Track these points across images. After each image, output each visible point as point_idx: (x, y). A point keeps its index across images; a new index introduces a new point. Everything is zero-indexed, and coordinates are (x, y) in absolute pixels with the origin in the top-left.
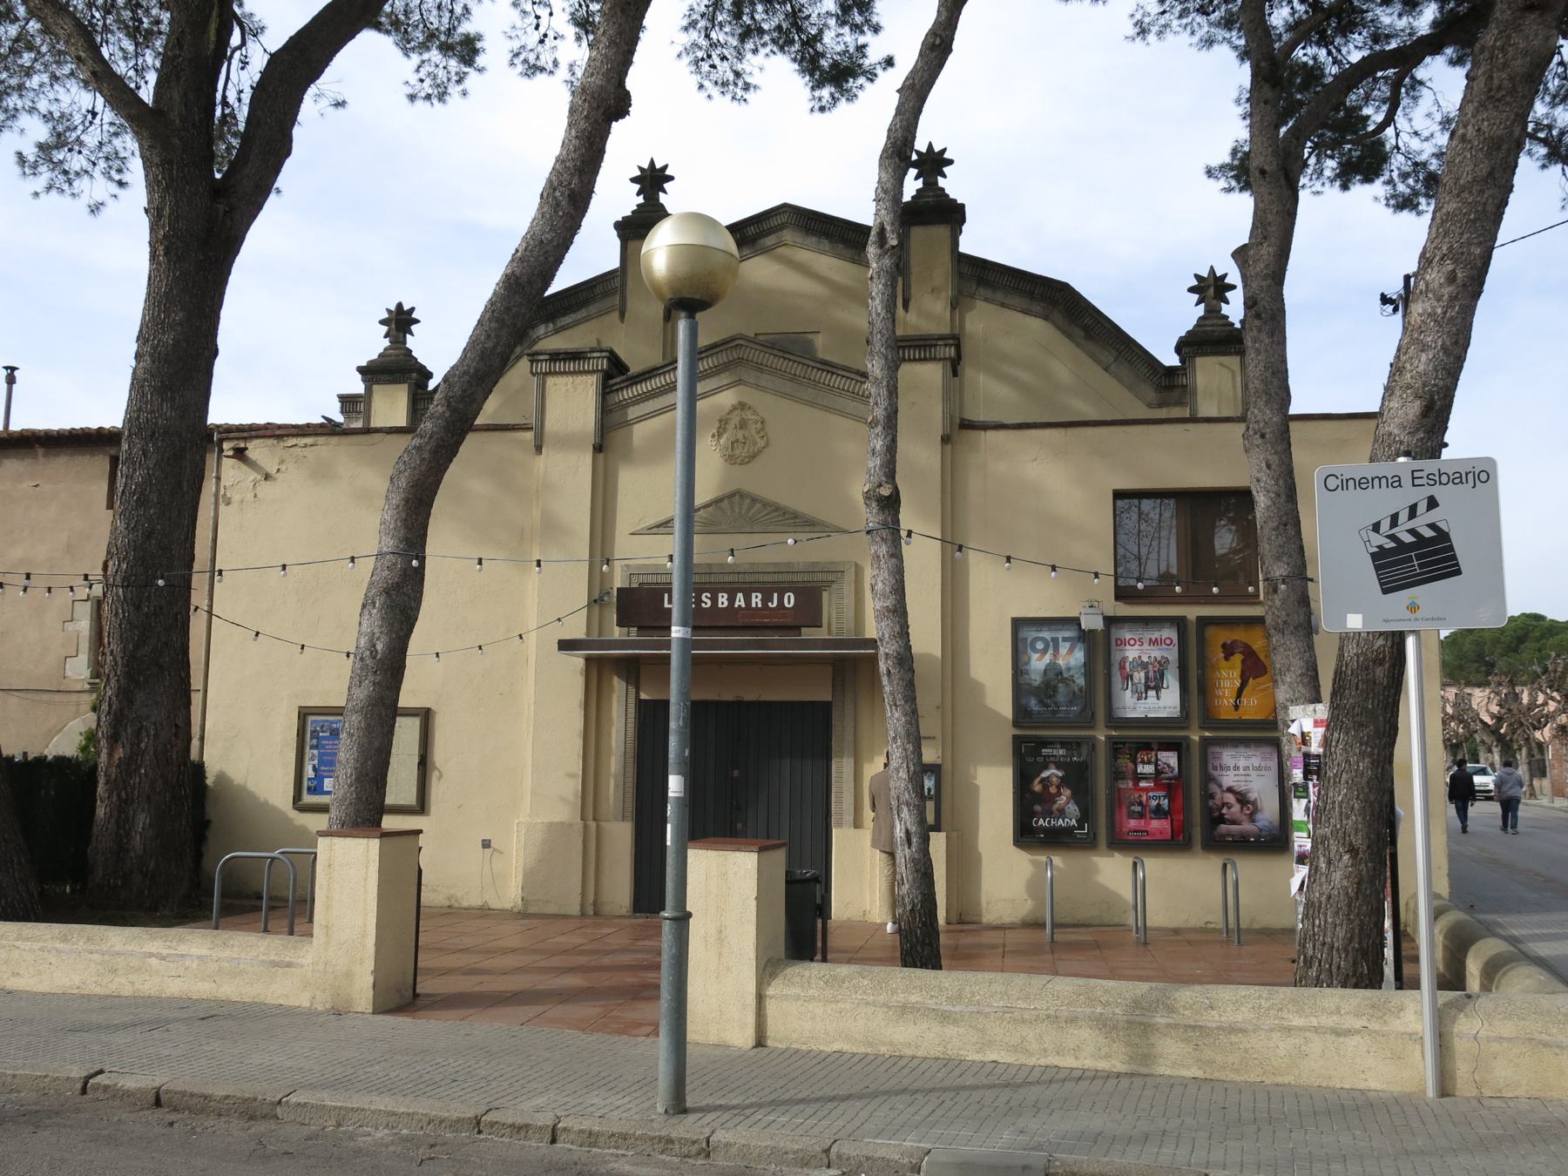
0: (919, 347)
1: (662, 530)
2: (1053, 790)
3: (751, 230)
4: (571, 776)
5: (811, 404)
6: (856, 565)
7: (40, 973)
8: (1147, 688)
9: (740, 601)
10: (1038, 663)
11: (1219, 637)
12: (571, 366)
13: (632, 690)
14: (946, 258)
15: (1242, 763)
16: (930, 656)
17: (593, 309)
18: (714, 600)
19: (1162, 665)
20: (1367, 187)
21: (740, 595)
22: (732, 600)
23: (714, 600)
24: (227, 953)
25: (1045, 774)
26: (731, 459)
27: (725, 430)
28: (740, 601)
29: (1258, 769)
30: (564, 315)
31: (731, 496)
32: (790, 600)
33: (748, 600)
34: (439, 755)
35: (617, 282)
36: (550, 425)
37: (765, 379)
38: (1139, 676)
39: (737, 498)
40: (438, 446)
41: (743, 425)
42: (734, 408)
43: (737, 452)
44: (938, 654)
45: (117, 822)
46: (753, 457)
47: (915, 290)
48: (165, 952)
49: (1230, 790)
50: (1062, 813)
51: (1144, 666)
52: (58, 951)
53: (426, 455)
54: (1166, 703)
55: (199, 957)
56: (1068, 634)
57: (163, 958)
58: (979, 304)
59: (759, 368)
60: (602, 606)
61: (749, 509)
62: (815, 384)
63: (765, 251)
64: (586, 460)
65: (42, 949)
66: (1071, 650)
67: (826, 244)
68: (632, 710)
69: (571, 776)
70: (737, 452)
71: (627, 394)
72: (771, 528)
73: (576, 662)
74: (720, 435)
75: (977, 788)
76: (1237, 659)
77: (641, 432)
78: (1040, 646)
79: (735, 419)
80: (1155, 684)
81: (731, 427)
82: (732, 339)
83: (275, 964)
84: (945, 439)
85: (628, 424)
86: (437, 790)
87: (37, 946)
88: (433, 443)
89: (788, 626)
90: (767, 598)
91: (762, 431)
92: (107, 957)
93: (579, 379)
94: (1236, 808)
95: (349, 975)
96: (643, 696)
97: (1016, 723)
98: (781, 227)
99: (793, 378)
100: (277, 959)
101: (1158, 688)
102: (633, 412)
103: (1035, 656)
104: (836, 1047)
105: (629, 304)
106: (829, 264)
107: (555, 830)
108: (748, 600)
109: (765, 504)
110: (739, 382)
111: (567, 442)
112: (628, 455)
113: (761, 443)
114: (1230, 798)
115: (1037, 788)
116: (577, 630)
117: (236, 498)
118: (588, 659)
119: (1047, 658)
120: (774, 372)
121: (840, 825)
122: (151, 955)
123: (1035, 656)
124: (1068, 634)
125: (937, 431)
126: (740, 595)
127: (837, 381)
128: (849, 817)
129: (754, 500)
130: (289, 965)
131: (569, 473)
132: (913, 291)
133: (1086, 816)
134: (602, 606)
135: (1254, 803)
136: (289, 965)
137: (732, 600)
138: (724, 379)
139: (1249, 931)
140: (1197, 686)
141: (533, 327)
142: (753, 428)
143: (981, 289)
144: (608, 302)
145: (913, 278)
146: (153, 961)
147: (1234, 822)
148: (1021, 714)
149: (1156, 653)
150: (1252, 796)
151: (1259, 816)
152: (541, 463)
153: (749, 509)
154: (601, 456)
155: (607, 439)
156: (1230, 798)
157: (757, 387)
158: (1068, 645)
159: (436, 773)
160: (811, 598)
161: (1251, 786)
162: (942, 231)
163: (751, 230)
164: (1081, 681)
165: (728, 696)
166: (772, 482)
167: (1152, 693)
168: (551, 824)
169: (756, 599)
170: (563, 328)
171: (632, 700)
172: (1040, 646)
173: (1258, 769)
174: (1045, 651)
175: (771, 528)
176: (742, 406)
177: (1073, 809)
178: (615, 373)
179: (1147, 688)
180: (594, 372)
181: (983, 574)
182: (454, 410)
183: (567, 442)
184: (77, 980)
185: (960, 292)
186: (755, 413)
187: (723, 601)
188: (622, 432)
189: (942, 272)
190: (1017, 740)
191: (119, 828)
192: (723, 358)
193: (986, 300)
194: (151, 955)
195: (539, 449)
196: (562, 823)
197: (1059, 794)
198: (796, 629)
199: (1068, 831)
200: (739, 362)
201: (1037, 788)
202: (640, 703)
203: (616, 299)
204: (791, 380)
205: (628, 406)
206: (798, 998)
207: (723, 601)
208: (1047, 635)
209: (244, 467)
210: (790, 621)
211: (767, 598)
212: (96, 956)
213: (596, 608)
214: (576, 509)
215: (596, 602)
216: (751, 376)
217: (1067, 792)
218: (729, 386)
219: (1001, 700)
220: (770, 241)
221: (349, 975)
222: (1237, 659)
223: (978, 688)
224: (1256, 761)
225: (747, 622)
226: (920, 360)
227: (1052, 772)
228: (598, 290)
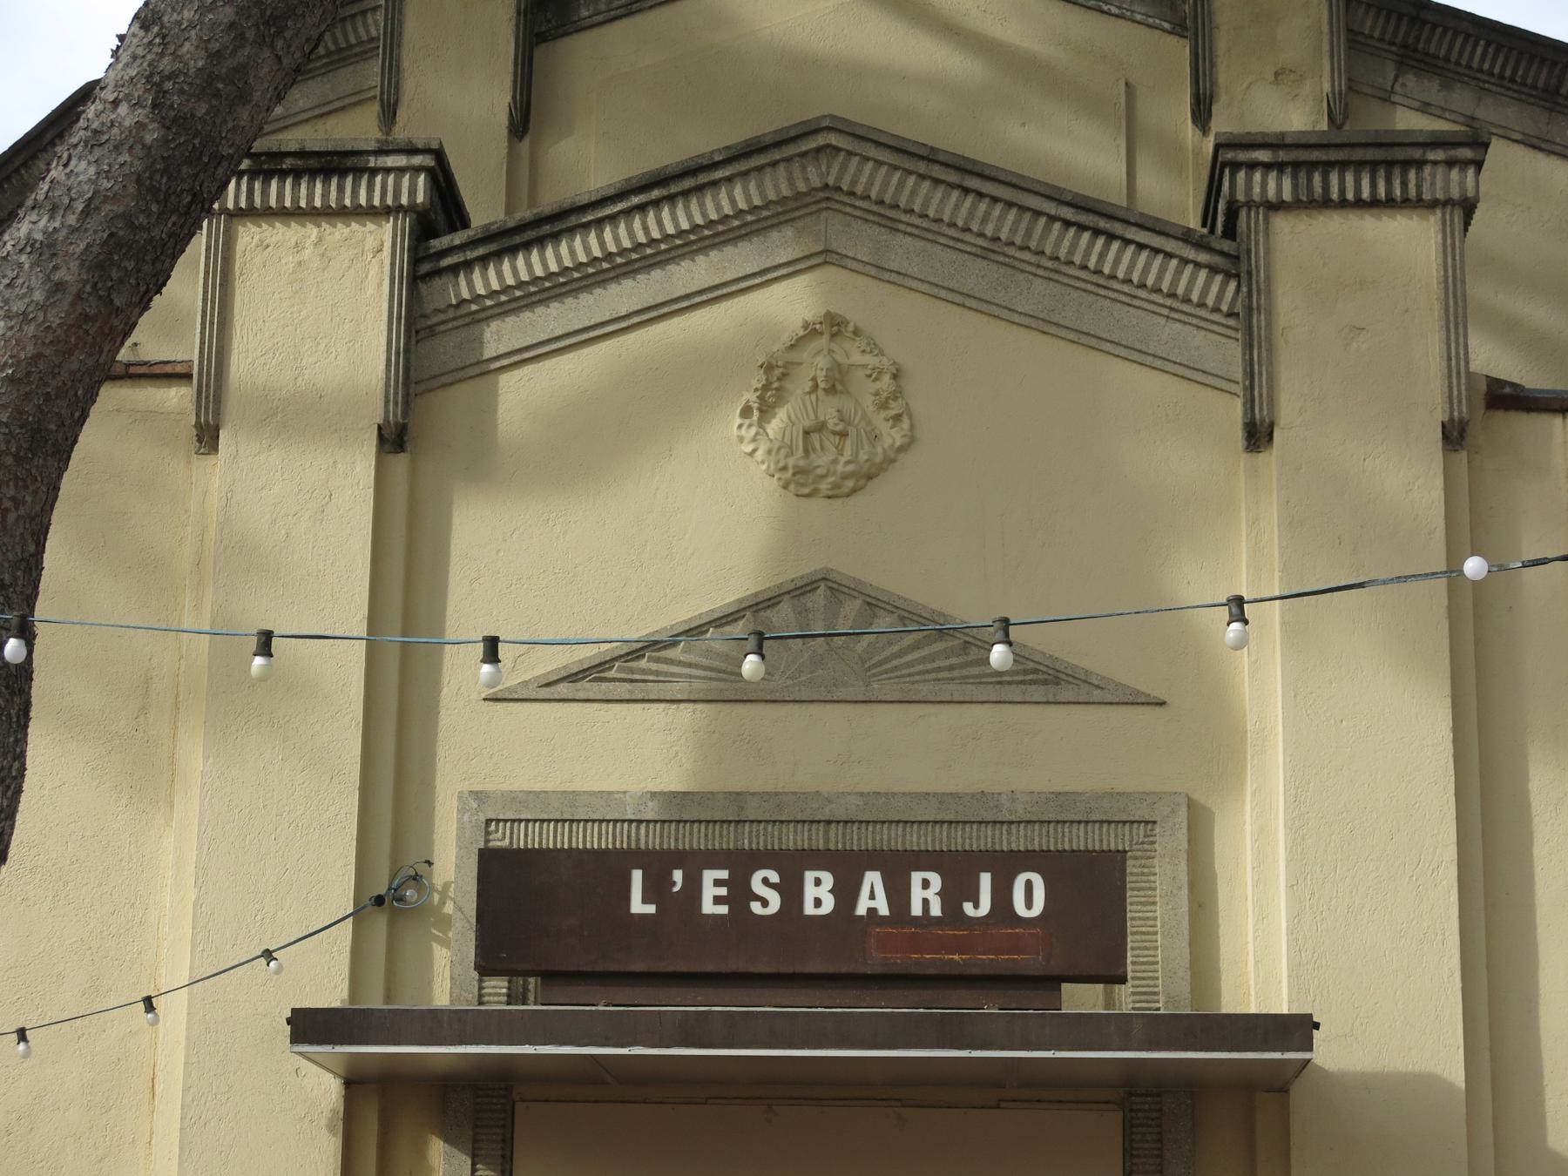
0: (1373, 165)
1: (586, 688)
5: (1043, 324)
6: (1192, 806)
9: (873, 896)
12: (316, 193)
16: (1430, 1082)
18: (791, 891)
21: (873, 879)
22: (846, 892)
23: (791, 891)
26: (800, 480)
27: (781, 396)
28: (873, 896)
32: (1031, 897)
33: (898, 893)
36: (243, 365)
37: (903, 251)
39: (820, 597)
40: (113, 244)
41: (836, 382)
42: (810, 332)
43: (821, 460)
44: (1456, 1073)
46: (868, 476)
53: (69, 273)
60: (395, 916)
62: (1057, 268)
64: (354, 471)
70: (821, 460)
71: (485, 281)
72: (925, 690)
73: (318, 1085)
74: (766, 411)
77: (522, 398)
79: (815, 362)
81: (799, 386)
82: (809, 130)
84: (1454, 436)
85: (484, 370)
88: (96, 231)
89: (1019, 975)
90: (958, 890)
91: (894, 401)
93: (339, 232)
99: (990, 249)
102: (499, 337)
108: (898, 893)
109: (908, 615)
110: (825, 257)
111: (298, 416)
112: (482, 461)
113: (892, 436)
116: (329, 989)
118: (355, 1082)
120: (932, 229)
125: (1430, 409)
126: (873, 879)
127: (1122, 261)
129: (874, 603)
131: (304, 510)
132: (1223, 75)
134: (395, 916)
137: (846, 892)
138: (782, 246)
142: (865, 393)
143: (1411, 80)
144: (346, 79)
145: (1222, 43)
152: (215, 476)
154: (400, 463)
155: (420, 416)
157: (879, 271)
160: (1094, 888)
166: (914, 551)
169: (926, 892)
175: (925, 690)
176: (833, 326)
178: (436, 231)
180: (386, 212)
182: (176, 123)
183: (298, 416)
185: (1352, 87)
186: (874, 348)
187: (819, 894)
188: (462, 394)
192: (777, 185)
195: (208, 437)
198: (1050, 982)
200: (828, 196)
204: (984, 254)
205: (482, 317)
207: (819, 894)
210: (1030, 962)
211: (958, 890)
213: (379, 923)
215: (388, 902)
216: (859, 240)
218: (792, 269)
225: (897, 961)
226: (1374, 204)
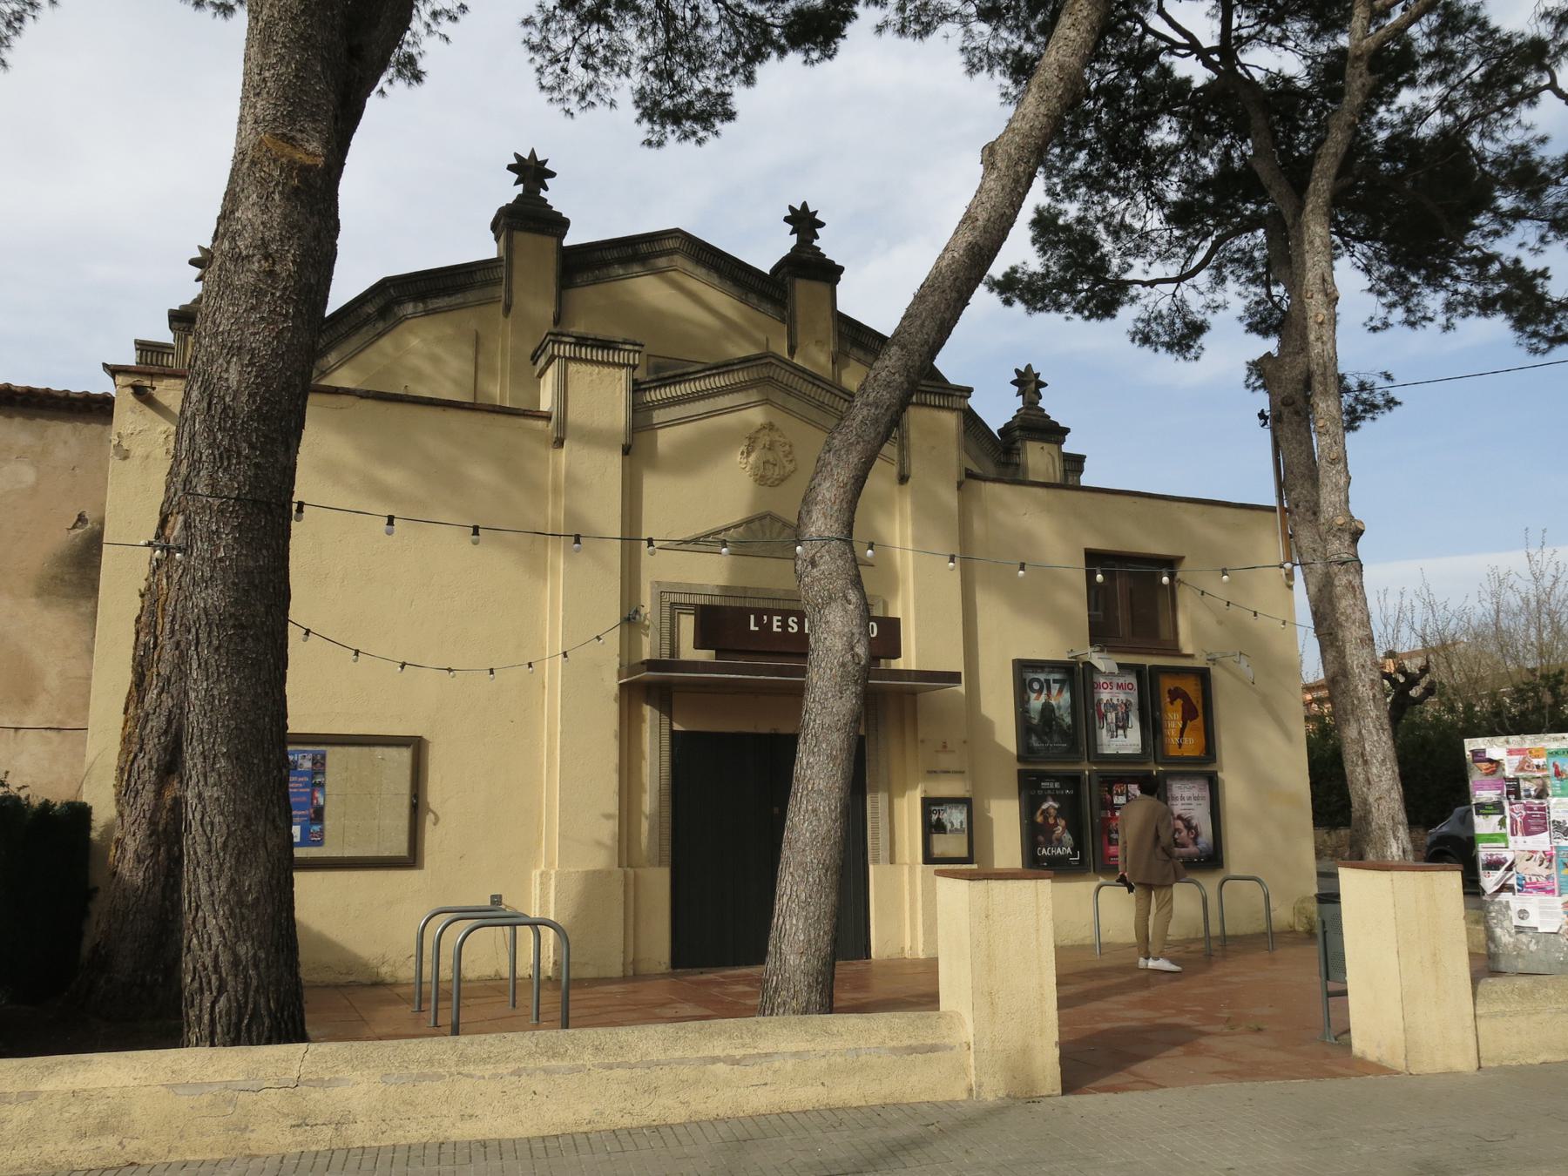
1: (691, 546)
2: (1051, 821)
3: (644, 248)
4: (608, 817)
7: (516, 1108)
8: (1118, 727)
10: (1036, 702)
11: (1167, 684)
12: (599, 355)
13: (666, 720)
14: (828, 313)
15: (1186, 794)
17: (471, 296)
19: (1127, 705)
20: (1483, 320)
24: (837, 1044)
25: (1045, 806)
29: (1196, 798)
30: (437, 297)
31: (761, 518)
34: (435, 794)
35: (503, 272)
37: (792, 403)
38: (1111, 716)
42: (763, 427)
45: (164, 888)
47: (800, 338)
48: (738, 1053)
49: (1180, 817)
50: (1060, 843)
51: (1114, 707)
52: (546, 1071)
54: (1129, 741)
55: (796, 1054)
56: (1057, 676)
57: (735, 1062)
58: (853, 363)
59: (788, 390)
61: (780, 534)
63: (658, 272)
65: (517, 1073)
66: (1060, 691)
67: (715, 279)
68: (666, 741)
69: (608, 817)
70: (769, 473)
74: (749, 454)
75: (991, 820)
76: (1179, 702)
78: (1036, 686)
80: (1122, 725)
83: (912, 1050)
84: (960, 485)
86: (432, 837)
87: (503, 1069)
92: (638, 1071)
94: (1185, 833)
95: (1026, 1051)
96: (677, 727)
97: (1020, 758)
98: (670, 252)
99: (820, 406)
100: (913, 1042)
101: (1124, 728)
102: (659, 416)
103: (1033, 696)
104: (1541, 1058)
105: (515, 300)
106: (723, 301)
107: (594, 880)
111: (593, 438)
113: (790, 467)
114: (1180, 824)
115: (1040, 819)
117: (138, 451)
119: (1043, 698)
120: (801, 396)
121: (876, 861)
122: (715, 1060)
123: (1033, 696)
124: (1057, 676)
128: (884, 854)
130: (933, 1049)
133: (1078, 845)
135: (1196, 828)
136: (933, 1049)
138: (754, 396)
139: (1235, 937)
140: (1152, 728)
141: (400, 303)
145: (799, 327)
146: (721, 1068)
147: (1184, 846)
148: (1025, 753)
149: (1122, 697)
150: (1194, 822)
151: (1200, 840)
153: (780, 534)
156: (1180, 824)
157: (784, 409)
158: (1057, 686)
159: (430, 818)
161: (1193, 813)
162: (820, 288)
163: (644, 248)
164: (1068, 720)
165: (764, 728)
167: (1120, 732)
168: (587, 873)
170: (435, 311)
171: (666, 731)
172: (1036, 686)
173: (1196, 798)
174: (1040, 691)
176: (770, 427)
177: (1067, 837)
179: (1118, 727)
180: (623, 366)
181: (992, 613)
183: (593, 438)
184: (586, 1111)
189: (826, 326)
190: (1022, 775)
191: (164, 898)
192: (754, 374)
193: (859, 360)
194: (715, 1060)
196: (600, 872)
197: (1056, 825)
199: (1064, 858)
200: (769, 380)
201: (1040, 819)
202: (673, 733)
203: (501, 292)
204: (818, 407)
206: (1503, 1014)
208: (1042, 677)
209: (149, 411)
212: (619, 1072)
214: (606, 516)
216: (778, 397)
217: (1062, 823)
218: (755, 404)
219: (1007, 736)
220: (662, 262)
221: (1026, 1051)
222: (1179, 702)
223: (987, 726)
224: (1195, 792)
227: (1049, 804)
228: (479, 276)
